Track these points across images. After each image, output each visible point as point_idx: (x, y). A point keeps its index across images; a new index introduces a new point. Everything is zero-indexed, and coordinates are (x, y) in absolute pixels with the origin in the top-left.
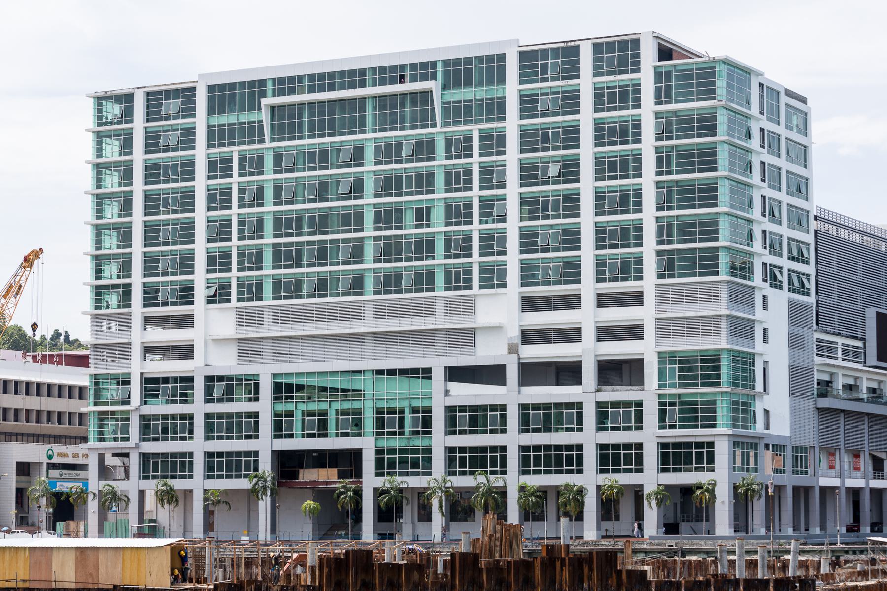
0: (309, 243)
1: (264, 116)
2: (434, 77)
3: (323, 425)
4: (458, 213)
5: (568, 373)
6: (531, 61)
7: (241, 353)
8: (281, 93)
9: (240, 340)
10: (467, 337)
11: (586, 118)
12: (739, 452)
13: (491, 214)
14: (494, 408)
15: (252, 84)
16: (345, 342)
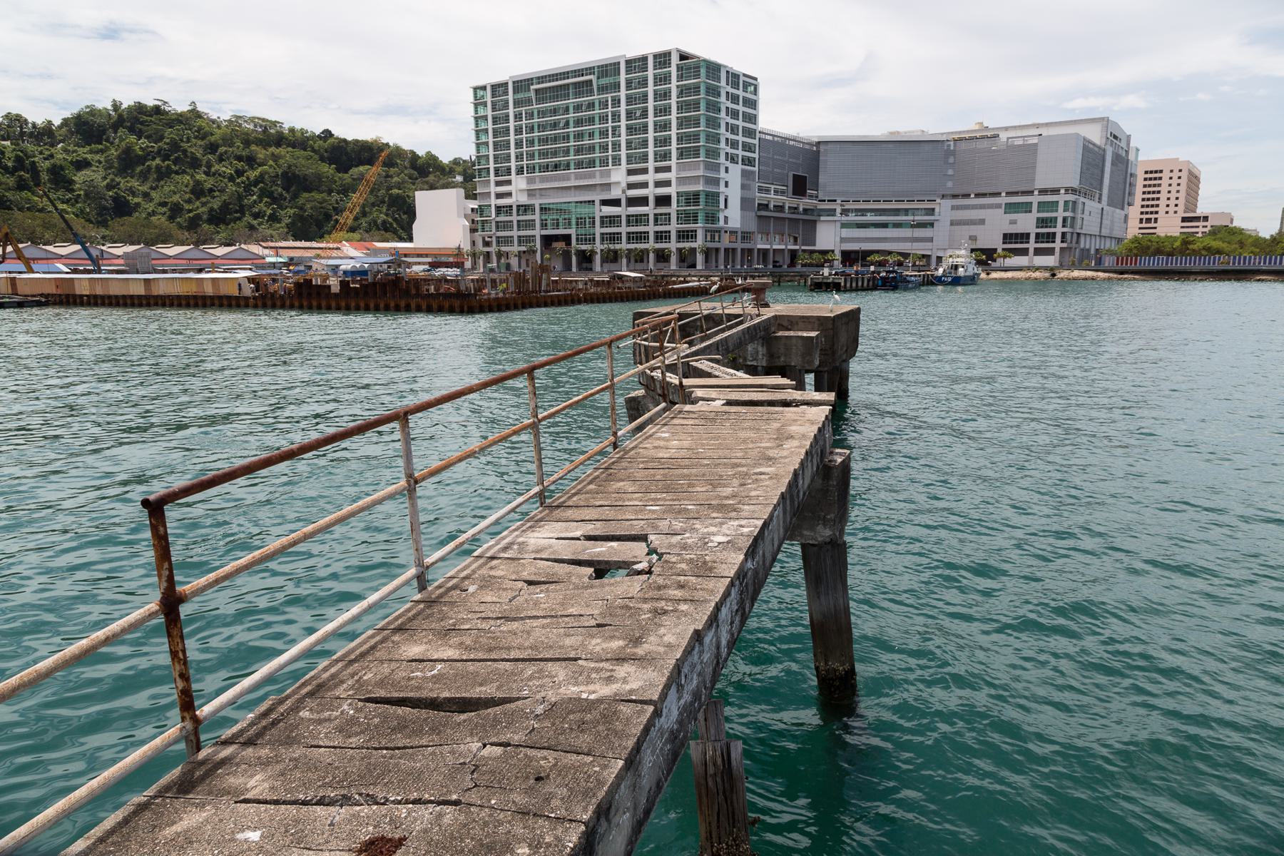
1: (532, 94)
4: (604, 133)
5: (643, 201)
10: (608, 186)
11: (651, 89)
16: (565, 190)
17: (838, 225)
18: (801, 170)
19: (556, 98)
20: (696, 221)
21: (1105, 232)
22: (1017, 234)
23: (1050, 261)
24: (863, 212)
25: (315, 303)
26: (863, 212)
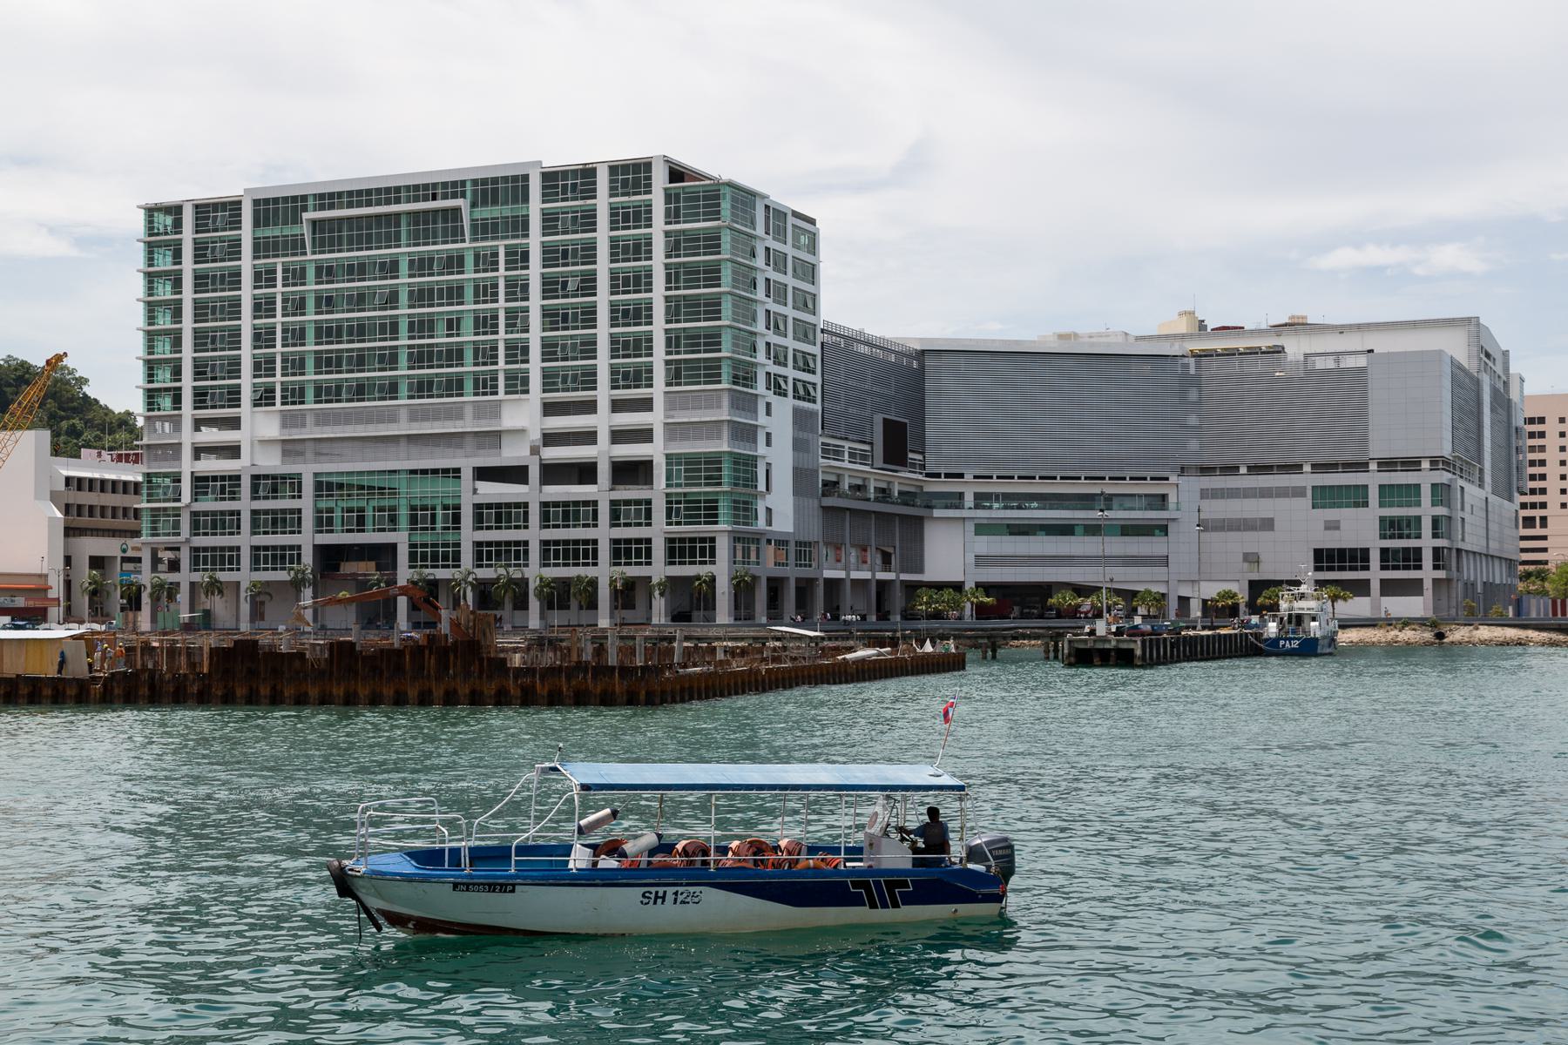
0: (348, 350)
1: (306, 230)
2: (463, 195)
3: (361, 521)
4: (486, 323)
5: (585, 472)
6: (552, 179)
7: (285, 453)
8: (322, 208)
9: (284, 441)
12: (739, 546)
13: (514, 325)
14: (517, 505)
15: (294, 199)
16: (384, 439)
17: (970, 527)
18: (893, 402)
19: (368, 243)
20: (712, 518)
21: (1494, 548)
22: (1342, 552)
23: (1414, 606)
24: (1021, 500)
25: (265, 691)
26: (1021, 500)
